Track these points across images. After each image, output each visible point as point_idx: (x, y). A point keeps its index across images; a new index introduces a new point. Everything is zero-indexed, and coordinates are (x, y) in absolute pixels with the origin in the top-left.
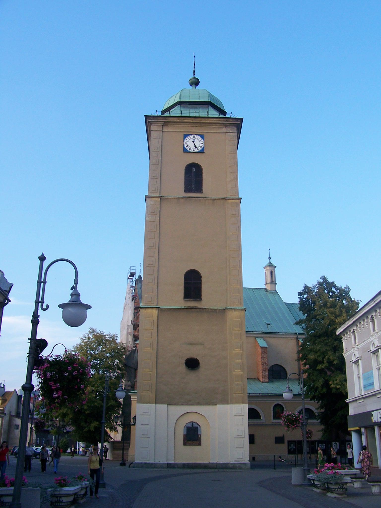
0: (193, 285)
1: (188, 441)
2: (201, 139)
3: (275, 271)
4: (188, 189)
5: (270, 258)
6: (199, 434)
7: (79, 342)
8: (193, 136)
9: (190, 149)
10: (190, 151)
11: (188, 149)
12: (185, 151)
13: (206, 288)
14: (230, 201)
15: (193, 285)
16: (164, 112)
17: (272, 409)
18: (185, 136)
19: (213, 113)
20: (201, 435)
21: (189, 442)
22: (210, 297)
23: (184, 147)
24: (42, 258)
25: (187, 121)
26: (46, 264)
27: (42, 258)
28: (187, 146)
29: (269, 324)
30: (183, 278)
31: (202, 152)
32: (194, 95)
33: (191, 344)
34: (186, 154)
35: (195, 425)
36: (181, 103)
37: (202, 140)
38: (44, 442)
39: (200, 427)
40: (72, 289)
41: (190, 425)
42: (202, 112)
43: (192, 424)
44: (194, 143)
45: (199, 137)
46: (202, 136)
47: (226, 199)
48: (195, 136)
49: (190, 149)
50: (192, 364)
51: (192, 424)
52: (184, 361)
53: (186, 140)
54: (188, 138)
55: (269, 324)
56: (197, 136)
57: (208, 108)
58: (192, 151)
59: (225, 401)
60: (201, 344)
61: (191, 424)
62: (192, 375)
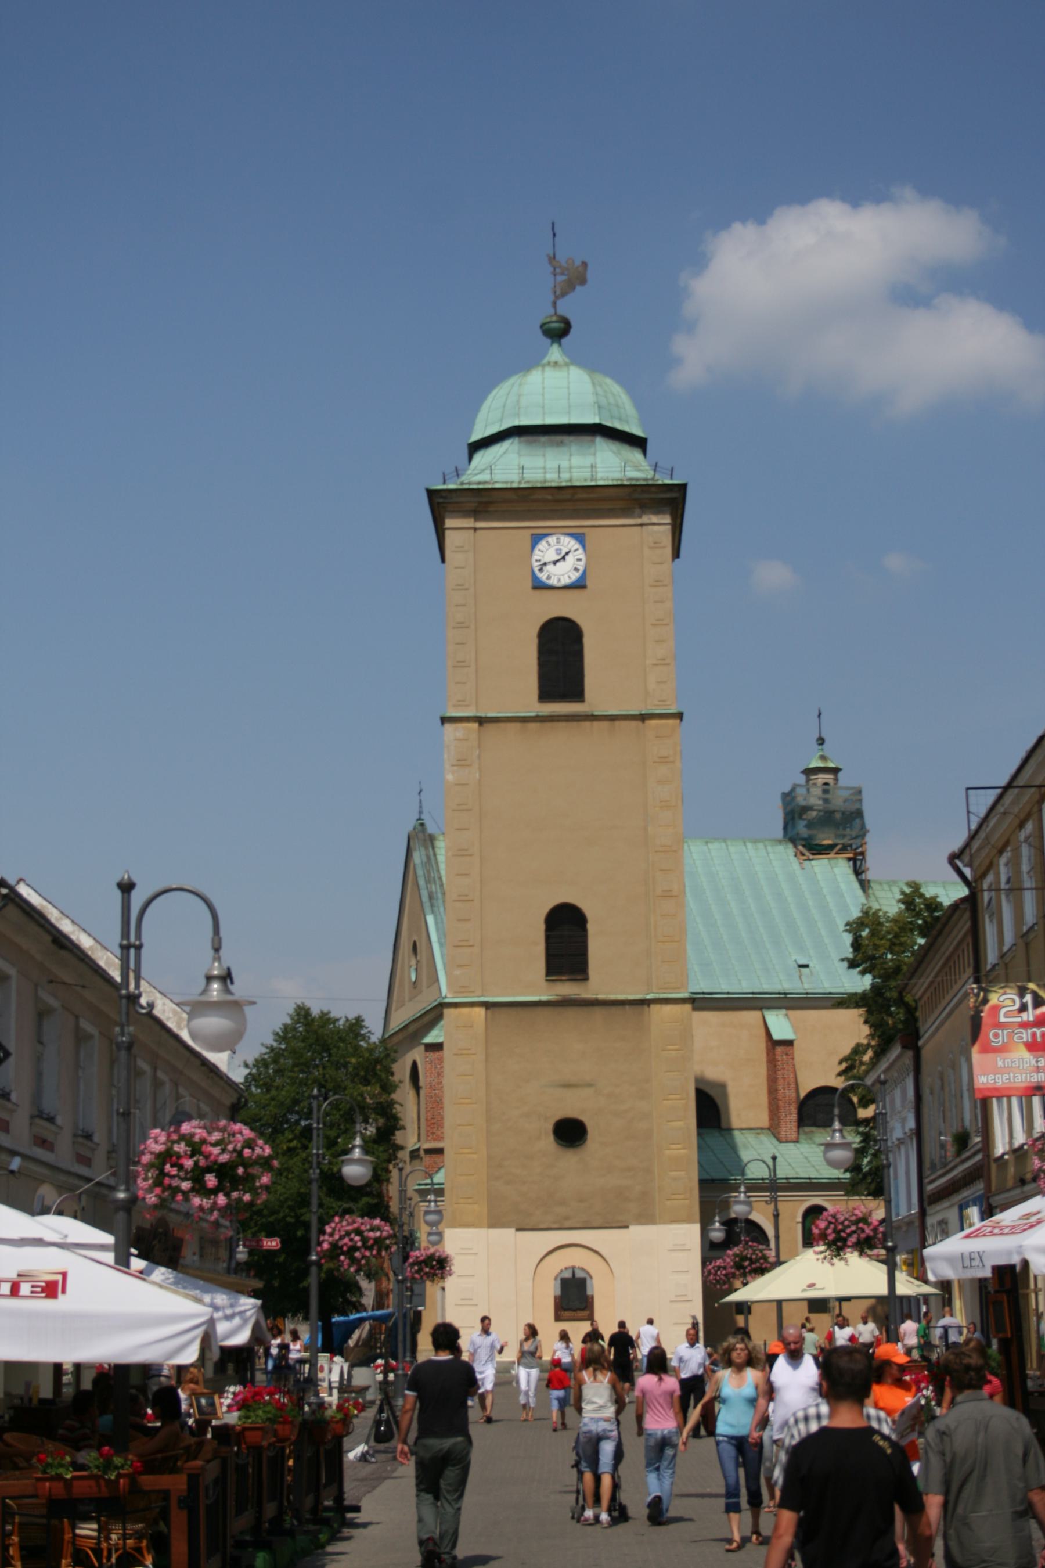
0: (566, 936)
1: (565, 1310)
2: (577, 546)
4: (546, 694)
5: (821, 741)
6: (589, 1293)
9: (549, 578)
12: (539, 586)
13: (599, 947)
14: (654, 722)
15: (566, 936)
17: (800, 1219)
18: (536, 539)
20: (592, 1297)
21: (567, 1314)
22: (608, 972)
24: (126, 888)
25: (540, 497)
26: (137, 898)
27: (126, 888)
29: (807, 966)
30: (542, 927)
31: (579, 585)
33: (568, 1086)
34: (538, 592)
35: (580, 1274)
37: (581, 551)
38: (342, 1318)
39: (591, 1278)
41: (568, 1275)
43: (574, 1274)
44: (559, 556)
46: (580, 538)
47: (643, 717)
48: (562, 538)
49: (549, 578)
50: (570, 1132)
51: (574, 1274)
52: (549, 1126)
53: (536, 552)
54: (542, 545)
55: (807, 966)
57: (593, 442)
59: (647, 1218)
60: (590, 1085)
61: (570, 1271)
62: (570, 1159)
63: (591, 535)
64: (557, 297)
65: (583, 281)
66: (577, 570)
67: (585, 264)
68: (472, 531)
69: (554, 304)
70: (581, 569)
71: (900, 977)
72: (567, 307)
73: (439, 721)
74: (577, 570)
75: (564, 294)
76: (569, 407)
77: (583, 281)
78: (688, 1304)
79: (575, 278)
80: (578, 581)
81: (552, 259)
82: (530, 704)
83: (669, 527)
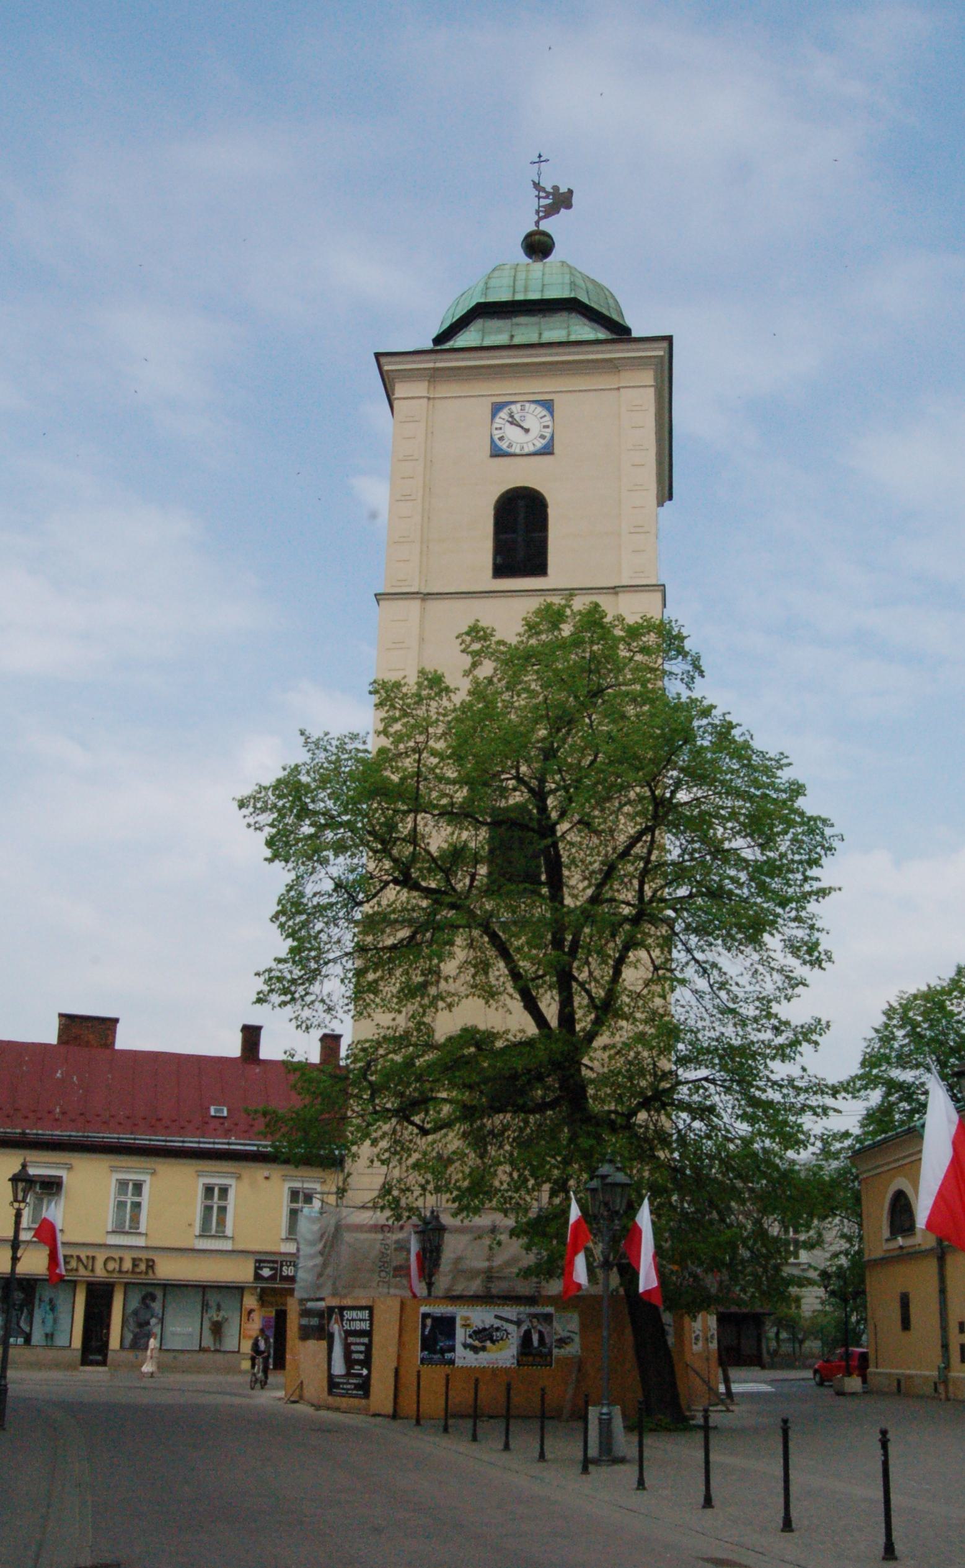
2: (544, 412)
3: (259, 1253)
4: (501, 570)
7: (482, 1027)
8: (518, 406)
9: (510, 446)
10: (512, 450)
11: (504, 445)
12: (497, 453)
16: (439, 339)
18: (497, 408)
19: (585, 331)
23: (492, 441)
28: (501, 439)
31: (547, 451)
32: (543, 280)
36: (484, 311)
37: (548, 418)
40: (71, 1024)
42: (555, 329)
45: (539, 409)
48: (527, 405)
49: (510, 446)
56: (533, 406)
58: (518, 451)
63: (561, 403)
64: (540, 219)
65: (569, 206)
66: (543, 437)
67: (570, 192)
68: (426, 400)
69: (537, 223)
70: (548, 436)
71: (817, 1252)
72: (545, 226)
73: (892, 1564)
74: (543, 437)
75: (545, 217)
76: (543, 285)
77: (569, 206)
78: (481, 1385)
79: (561, 201)
80: (545, 447)
81: (536, 185)
82: (485, 579)
83: (652, 390)
